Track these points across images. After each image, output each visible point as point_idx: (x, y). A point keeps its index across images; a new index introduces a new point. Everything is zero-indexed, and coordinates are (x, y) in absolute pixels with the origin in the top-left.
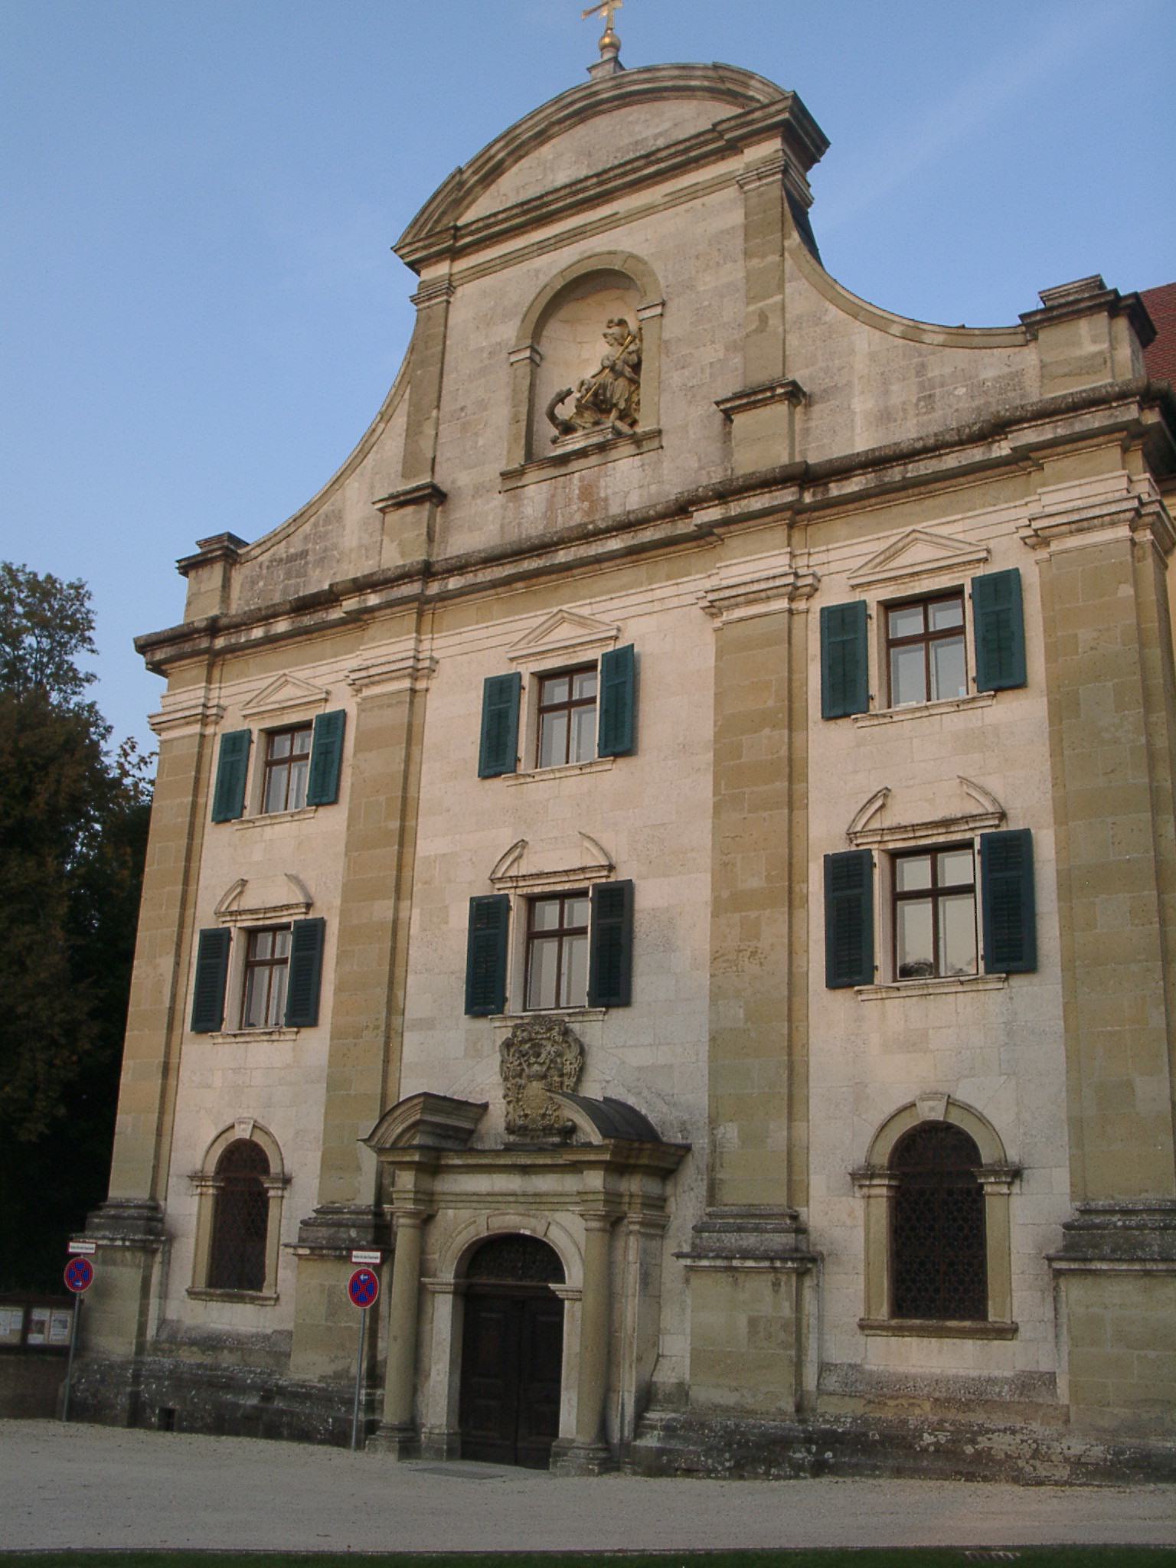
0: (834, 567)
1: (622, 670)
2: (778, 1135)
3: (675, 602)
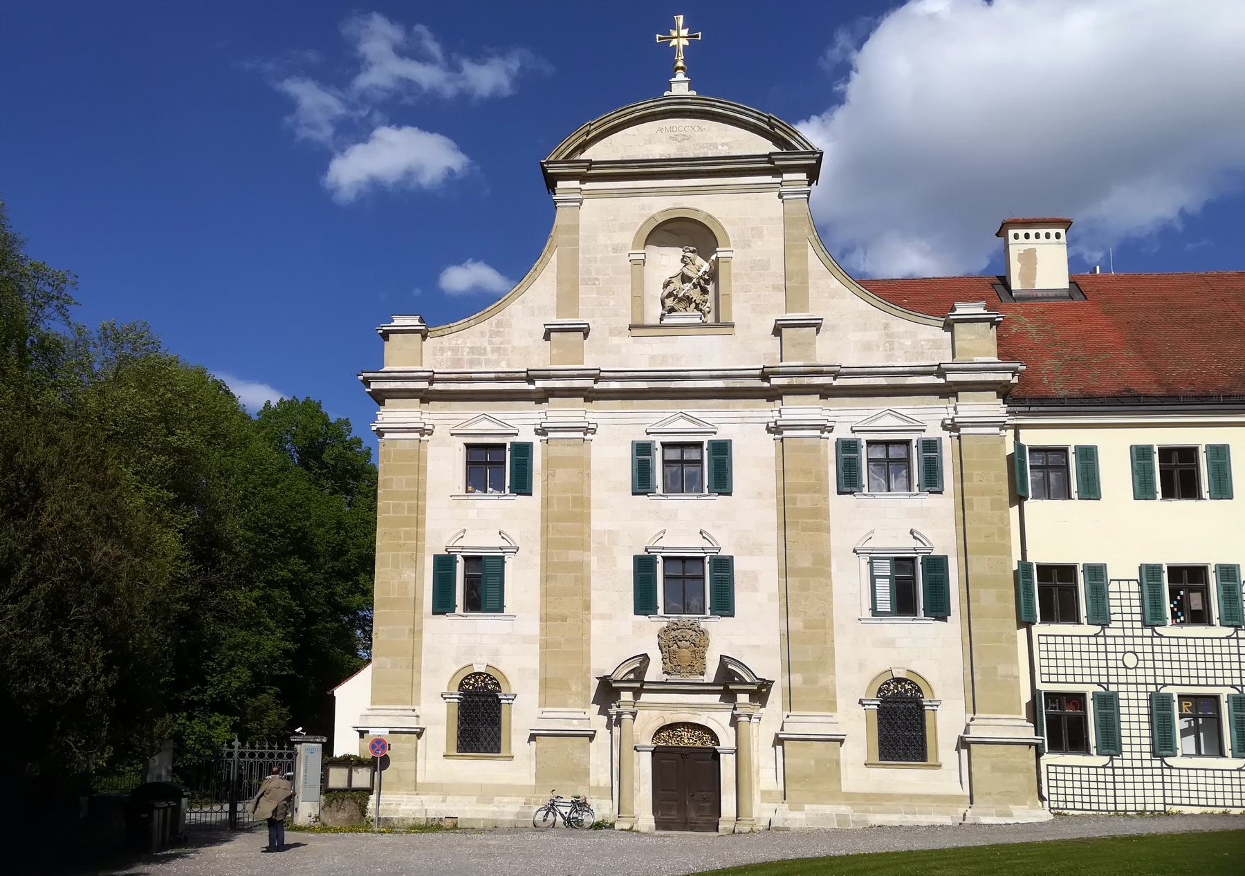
0: (842, 419)
1: (721, 450)
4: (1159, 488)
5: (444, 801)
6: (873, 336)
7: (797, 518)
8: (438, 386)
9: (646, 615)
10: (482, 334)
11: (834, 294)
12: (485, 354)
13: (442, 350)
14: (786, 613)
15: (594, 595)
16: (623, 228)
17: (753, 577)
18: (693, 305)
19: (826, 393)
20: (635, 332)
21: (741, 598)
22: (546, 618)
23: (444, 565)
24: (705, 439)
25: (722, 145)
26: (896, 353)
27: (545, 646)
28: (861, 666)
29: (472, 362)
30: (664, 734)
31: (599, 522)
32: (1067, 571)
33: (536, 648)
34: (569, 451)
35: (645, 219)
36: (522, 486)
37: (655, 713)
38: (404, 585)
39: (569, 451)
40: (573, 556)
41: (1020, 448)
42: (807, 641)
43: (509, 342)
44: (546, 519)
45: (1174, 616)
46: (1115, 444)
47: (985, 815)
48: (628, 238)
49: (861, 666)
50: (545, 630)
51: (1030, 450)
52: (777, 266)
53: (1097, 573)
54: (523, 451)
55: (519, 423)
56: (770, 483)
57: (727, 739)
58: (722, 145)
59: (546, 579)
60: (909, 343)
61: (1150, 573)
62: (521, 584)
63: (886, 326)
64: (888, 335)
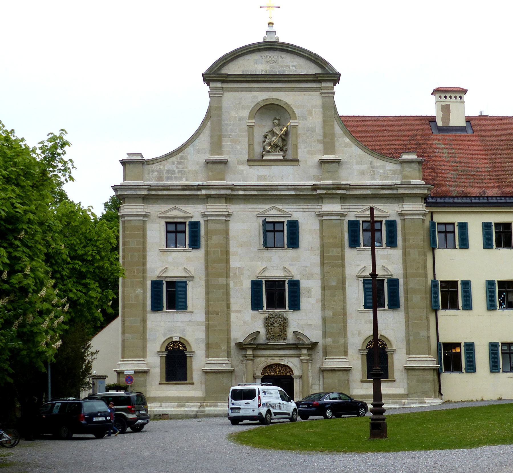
0: (351, 210)
1: (294, 226)
2: (342, 341)
3: (307, 210)
4: (494, 243)
5: (161, 406)
6: (365, 167)
7: (331, 263)
8: (153, 193)
9: (258, 310)
10: (173, 163)
11: (346, 145)
12: (175, 174)
13: (153, 171)
14: (324, 308)
15: (232, 301)
16: (243, 108)
17: (309, 290)
18: (279, 148)
19: (343, 198)
20: (251, 163)
21: (304, 301)
22: (207, 313)
23: (156, 285)
24: (285, 220)
25: (292, 66)
26: (376, 176)
27: (208, 327)
28: (359, 333)
29: (168, 179)
30: (267, 370)
31: (234, 263)
32: (453, 284)
33: (203, 328)
34: (218, 226)
35: (255, 104)
36: (195, 244)
37: (263, 359)
38: (137, 297)
39: (218, 226)
40: (222, 281)
41: (433, 224)
42: (335, 322)
43: (186, 168)
44: (207, 261)
45: (500, 305)
46: (475, 223)
47: (413, 403)
48: (246, 113)
49: (359, 333)
50: (207, 319)
51: (438, 224)
52: (319, 130)
53: (466, 284)
54: (195, 226)
55: (194, 212)
56: (317, 243)
57: (296, 372)
58: (292, 66)
59: (207, 293)
60: (381, 171)
61: (490, 284)
62: (195, 295)
63: (371, 163)
64: (372, 167)
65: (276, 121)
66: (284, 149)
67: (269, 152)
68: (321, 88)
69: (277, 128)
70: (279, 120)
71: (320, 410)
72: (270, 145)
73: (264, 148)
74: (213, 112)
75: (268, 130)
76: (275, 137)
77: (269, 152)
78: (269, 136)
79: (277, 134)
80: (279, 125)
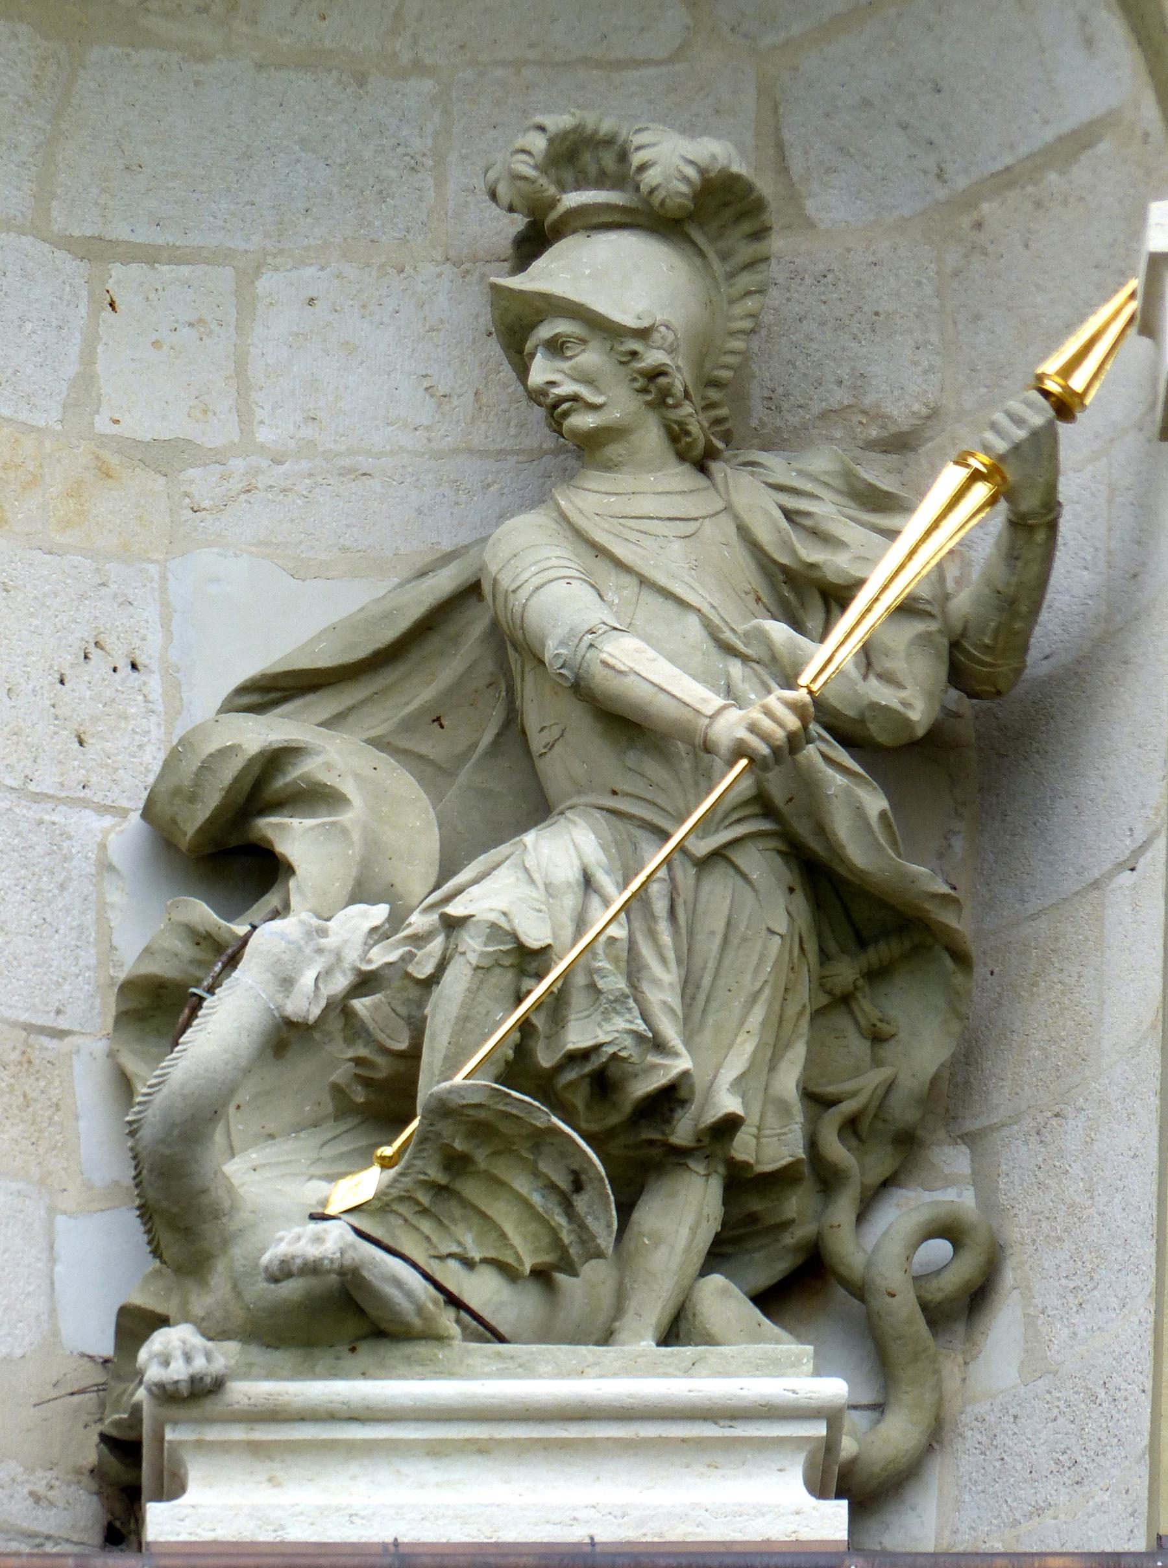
18: (684, 1212)
65: (620, 277)
66: (888, 1243)
67: (340, 1316)
68: (792, 939)
69: (644, 503)
70: (714, 217)
71: (512, 1358)
72: (381, 1099)
73: (173, 1207)
74: (365, 1207)
75: (310, 622)
76: (564, 848)
77: (340, 1316)
78: (366, 798)
79: (626, 726)
80: (707, 419)
